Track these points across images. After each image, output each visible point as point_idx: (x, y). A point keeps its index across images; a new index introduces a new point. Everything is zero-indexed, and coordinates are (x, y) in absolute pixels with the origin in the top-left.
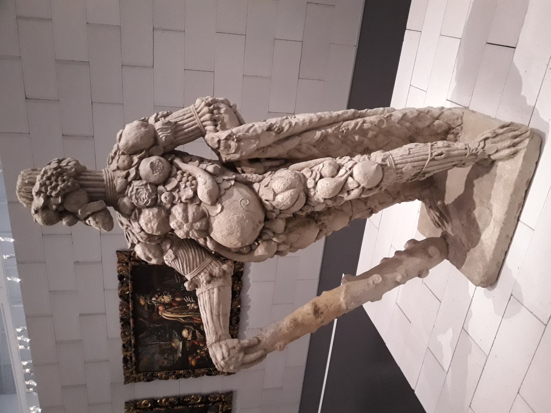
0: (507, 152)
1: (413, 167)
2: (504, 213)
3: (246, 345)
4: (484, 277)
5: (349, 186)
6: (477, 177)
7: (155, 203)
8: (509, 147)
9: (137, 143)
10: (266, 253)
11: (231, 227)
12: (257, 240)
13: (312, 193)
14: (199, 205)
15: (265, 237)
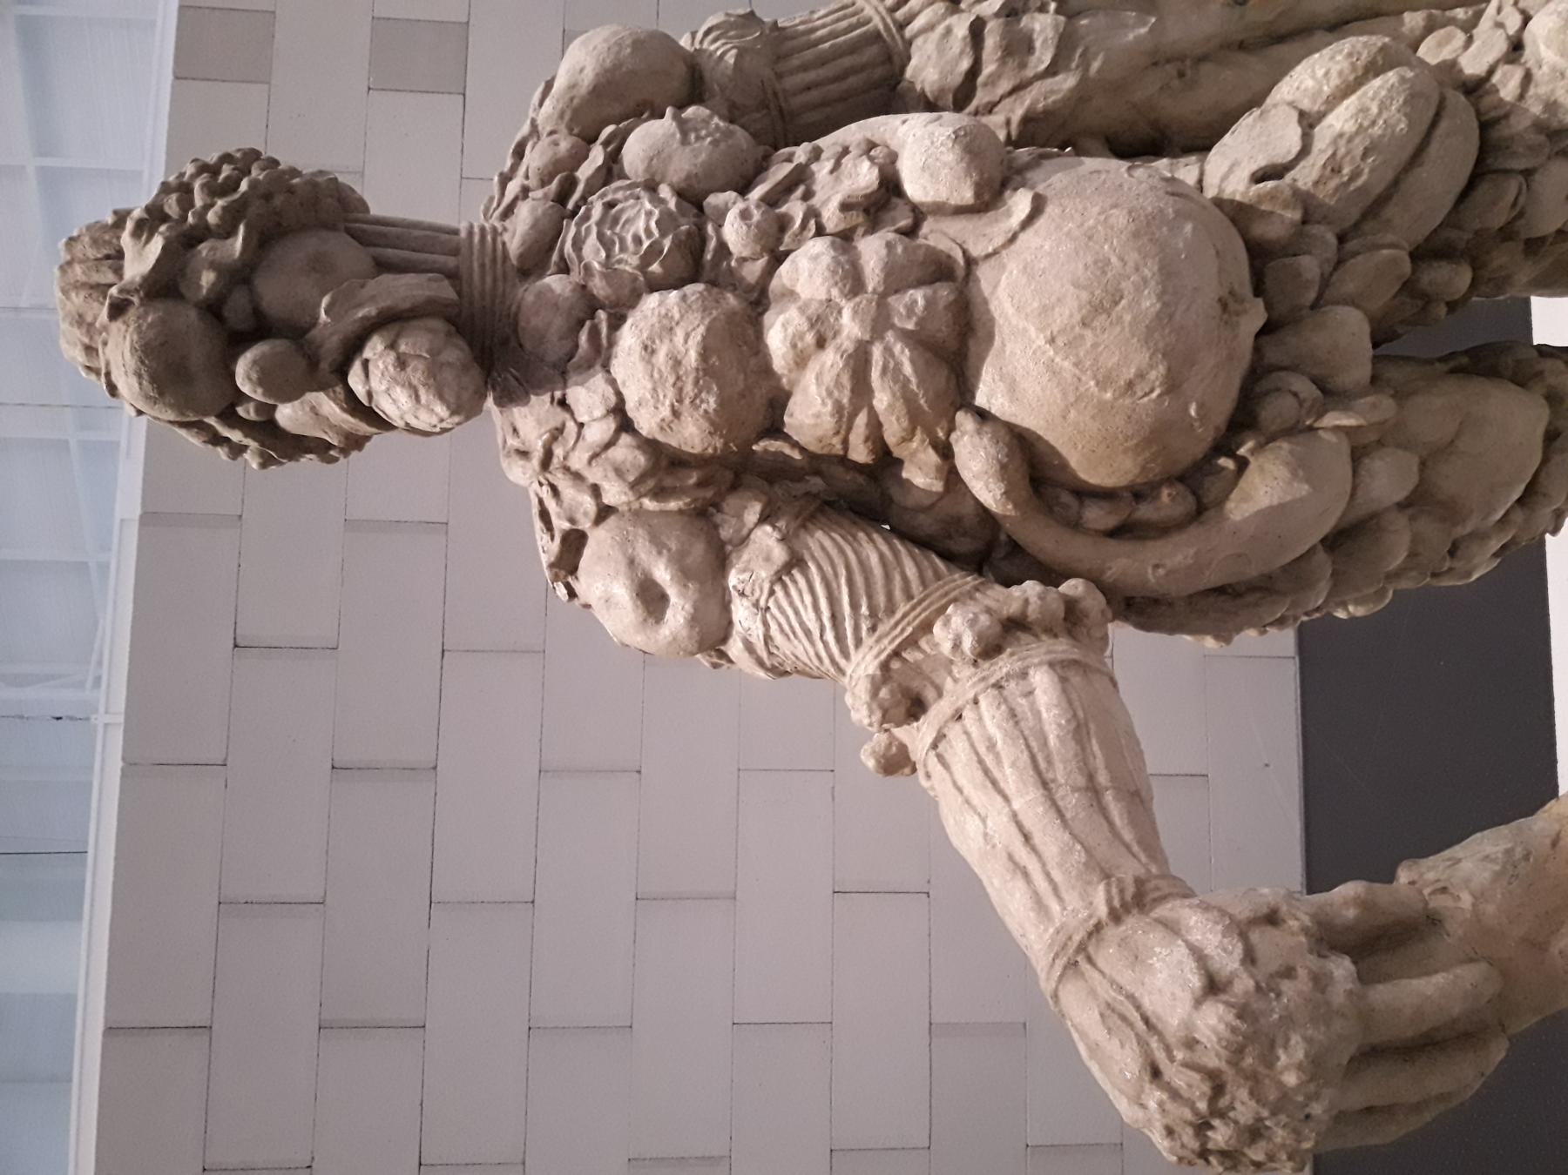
7: (692, 260)
9: (617, 66)
10: (1303, 489)
11: (1103, 264)
12: (1224, 445)
14: (911, 232)
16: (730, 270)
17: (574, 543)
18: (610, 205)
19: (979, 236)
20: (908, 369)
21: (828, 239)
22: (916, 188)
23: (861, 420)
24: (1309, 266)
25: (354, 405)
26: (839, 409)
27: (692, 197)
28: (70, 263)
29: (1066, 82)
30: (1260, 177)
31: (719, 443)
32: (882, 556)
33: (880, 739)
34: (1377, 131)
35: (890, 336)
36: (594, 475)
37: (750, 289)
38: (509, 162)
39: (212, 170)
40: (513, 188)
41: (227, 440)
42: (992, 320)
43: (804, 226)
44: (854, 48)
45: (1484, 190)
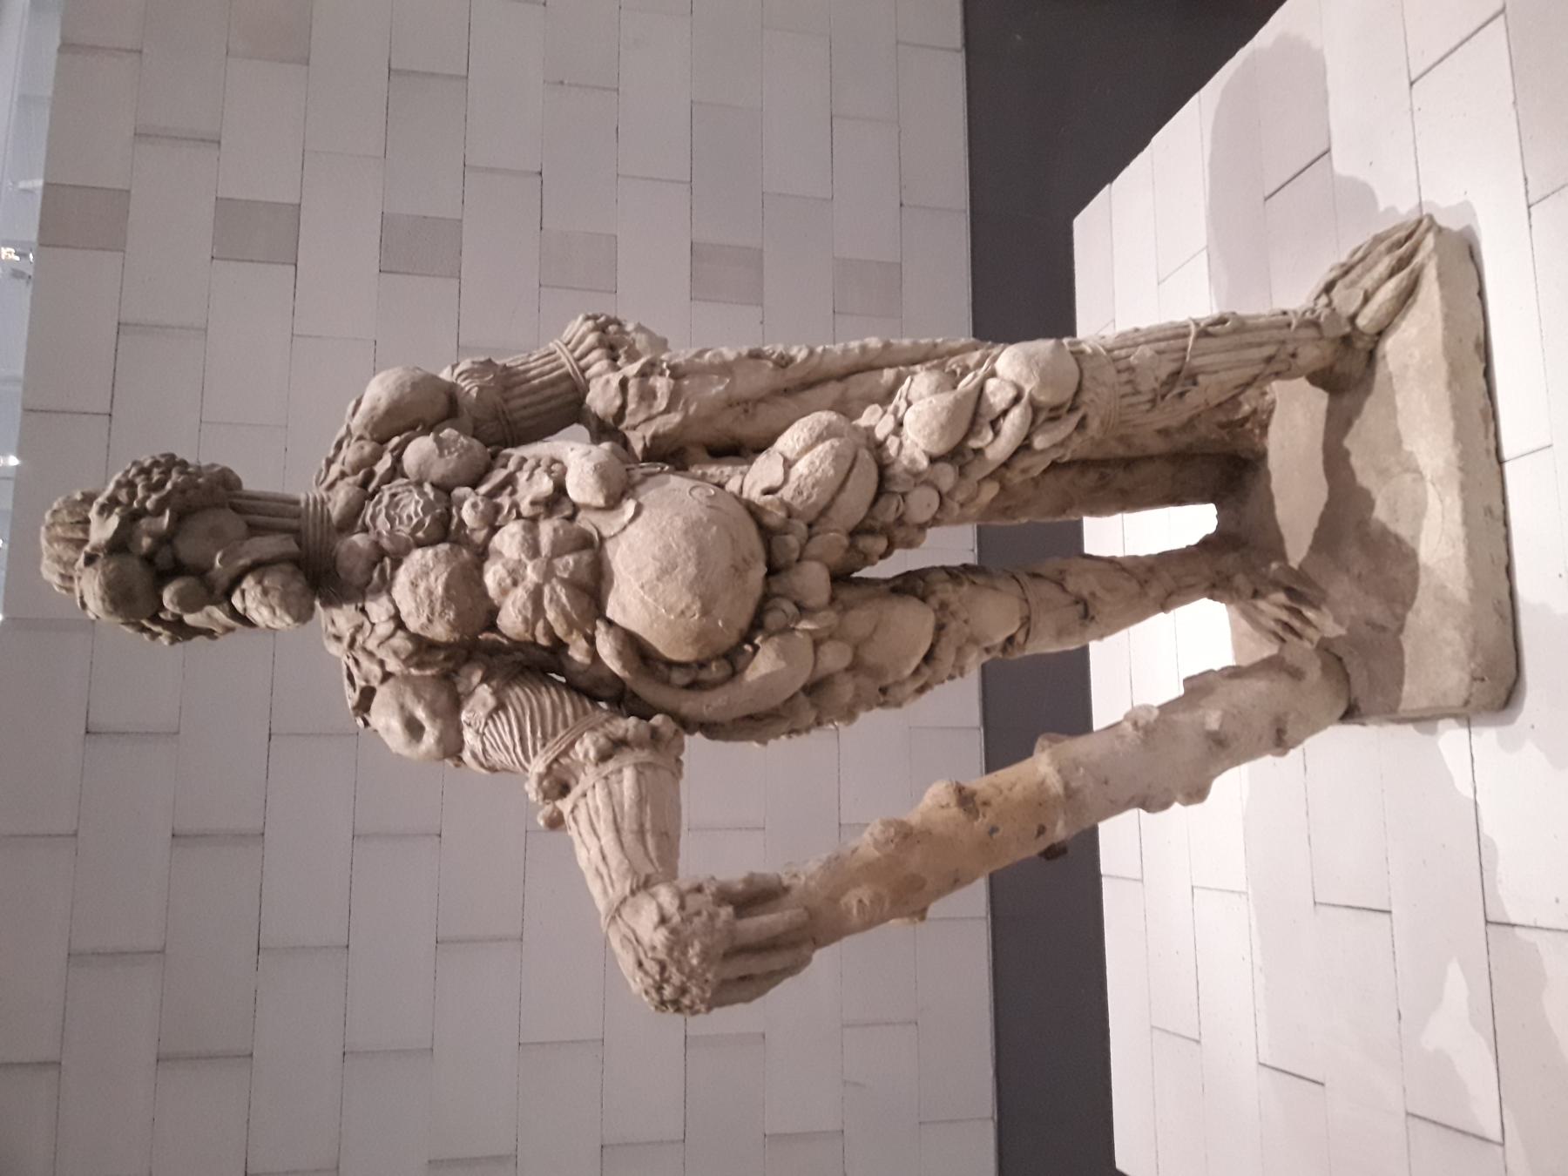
0: (1390, 287)
1: (1159, 352)
2: (1450, 441)
3: (740, 887)
4: (1472, 655)
5: (992, 400)
6: (1349, 424)
7: (443, 529)
8: (1391, 275)
9: (402, 397)
10: (782, 664)
12: (747, 638)
13: (893, 451)
14: (571, 518)
15: (773, 620)
16: (466, 536)
17: (368, 694)
18: (394, 495)
19: (608, 525)
20: (564, 599)
21: (521, 522)
22: (574, 493)
23: (540, 625)
24: (793, 541)
25: (234, 613)
26: (525, 620)
27: (444, 488)
28: (53, 525)
29: (676, 418)
30: (768, 492)
31: (457, 636)
32: (553, 703)
33: (548, 808)
34: (818, 474)
35: (554, 581)
36: (381, 654)
37: (478, 546)
38: (332, 452)
39: (145, 472)
40: (335, 470)
41: (149, 630)
42: (611, 573)
43: (509, 512)
44: (553, 383)
45: (882, 501)
